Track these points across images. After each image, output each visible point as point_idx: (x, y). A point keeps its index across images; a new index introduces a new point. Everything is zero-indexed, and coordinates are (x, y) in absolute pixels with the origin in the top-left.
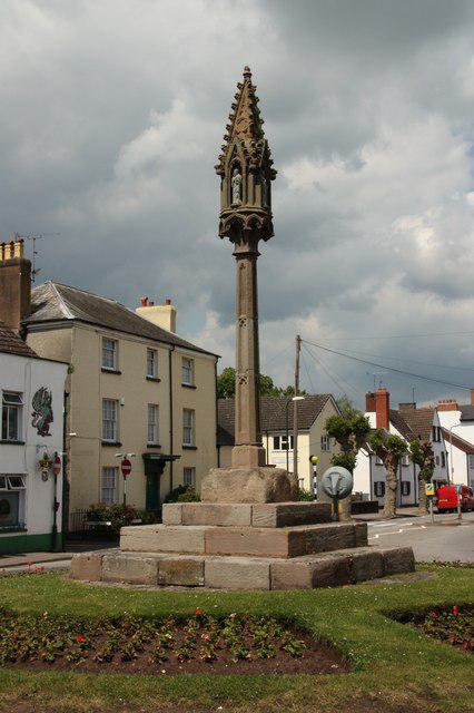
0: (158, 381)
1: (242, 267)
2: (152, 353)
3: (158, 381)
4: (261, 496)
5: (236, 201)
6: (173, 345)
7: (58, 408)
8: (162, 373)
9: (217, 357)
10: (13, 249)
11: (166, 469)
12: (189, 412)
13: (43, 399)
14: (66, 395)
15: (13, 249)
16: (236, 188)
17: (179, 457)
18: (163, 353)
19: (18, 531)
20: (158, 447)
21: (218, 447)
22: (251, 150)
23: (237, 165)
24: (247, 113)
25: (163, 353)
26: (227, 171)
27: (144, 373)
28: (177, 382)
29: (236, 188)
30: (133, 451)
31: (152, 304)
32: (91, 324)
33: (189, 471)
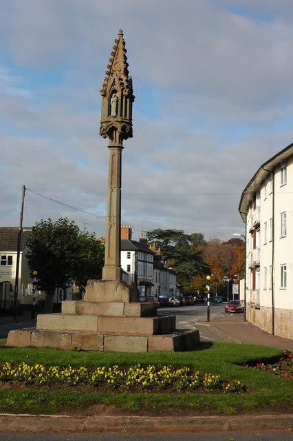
5: (113, 113)
22: (126, 84)
24: (120, 58)
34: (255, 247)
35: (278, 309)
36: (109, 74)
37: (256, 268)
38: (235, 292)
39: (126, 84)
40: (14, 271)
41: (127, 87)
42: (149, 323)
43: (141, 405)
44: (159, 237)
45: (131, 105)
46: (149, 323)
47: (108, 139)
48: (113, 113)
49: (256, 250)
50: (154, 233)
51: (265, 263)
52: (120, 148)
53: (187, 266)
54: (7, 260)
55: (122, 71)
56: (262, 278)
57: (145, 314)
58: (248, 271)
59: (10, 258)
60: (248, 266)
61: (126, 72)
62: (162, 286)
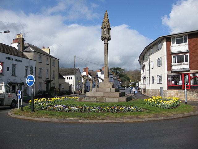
0: (48, 65)
1: (105, 46)
2: (47, 58)
3: (48, 65)
4: (111, 87)
5: (105, 34)
6: (51, 57)
7: (34, 69)
8: (49, 63)
9: (59, 60)
10: (20, 36)
11: (50, 83)
12: (54, 71)
13: (32, 68)
14: (36, 67)
15: (20, 36)
16: (105, 31)
17: (53, 81)
18: (49, 59)
19: (26, 95)
20: (48, 79)
21: (59, 79)
22: (108, 25)
23: (105, 27)
24: (106, 18)
25: (49, 59)
26: (103, 28)
27: (46, 63)
28: (52, 65)
29: (105, 31)
30: (44, 79)
31: (45, 48)
32: (37, 52)
33: (54, 83)
34: (144, 72)
35: (152, 90)
36: (103, 22)
37: (144, 78)
38: (137, 85)
39: (108, 25)
40: (3, 91)
41: (109, 26)
42: (118, 94)
43: (14, 88)
44: (114, 70)
45: (110, 31)
46: (118, 94)
47: (103, 41)
48: (105, 34)
49: (144, 73)
50: (113, 68)
51: (147, 76)
52: (107, 44)
53: (123, 78)
54: (70, 78)
55: (107, 22)
56: (147, 81)
57: (117, 91)
58: (142, 79)
59: (71, 77)
60: (142, 77)
61: (108, 22)
62: (116, 84)
